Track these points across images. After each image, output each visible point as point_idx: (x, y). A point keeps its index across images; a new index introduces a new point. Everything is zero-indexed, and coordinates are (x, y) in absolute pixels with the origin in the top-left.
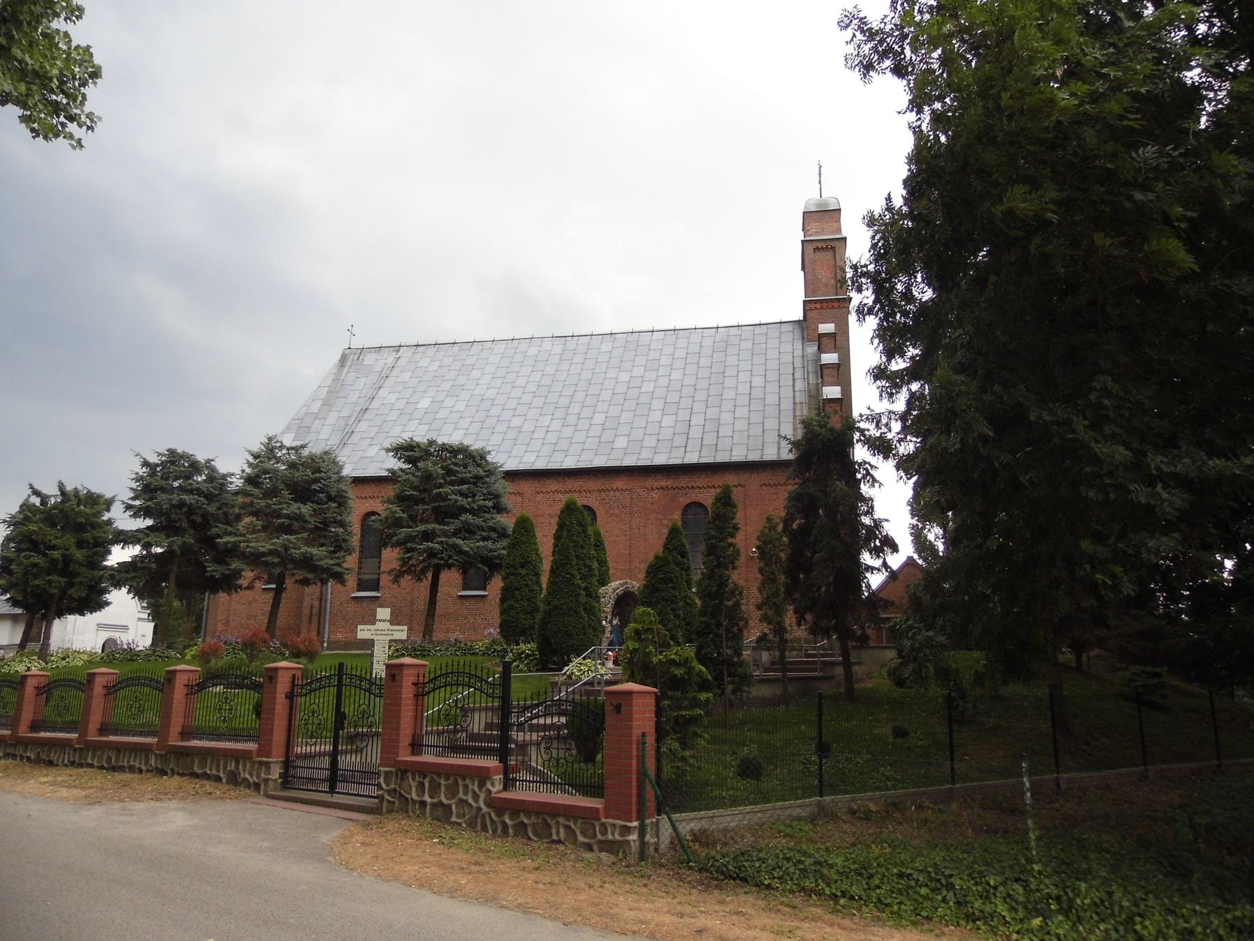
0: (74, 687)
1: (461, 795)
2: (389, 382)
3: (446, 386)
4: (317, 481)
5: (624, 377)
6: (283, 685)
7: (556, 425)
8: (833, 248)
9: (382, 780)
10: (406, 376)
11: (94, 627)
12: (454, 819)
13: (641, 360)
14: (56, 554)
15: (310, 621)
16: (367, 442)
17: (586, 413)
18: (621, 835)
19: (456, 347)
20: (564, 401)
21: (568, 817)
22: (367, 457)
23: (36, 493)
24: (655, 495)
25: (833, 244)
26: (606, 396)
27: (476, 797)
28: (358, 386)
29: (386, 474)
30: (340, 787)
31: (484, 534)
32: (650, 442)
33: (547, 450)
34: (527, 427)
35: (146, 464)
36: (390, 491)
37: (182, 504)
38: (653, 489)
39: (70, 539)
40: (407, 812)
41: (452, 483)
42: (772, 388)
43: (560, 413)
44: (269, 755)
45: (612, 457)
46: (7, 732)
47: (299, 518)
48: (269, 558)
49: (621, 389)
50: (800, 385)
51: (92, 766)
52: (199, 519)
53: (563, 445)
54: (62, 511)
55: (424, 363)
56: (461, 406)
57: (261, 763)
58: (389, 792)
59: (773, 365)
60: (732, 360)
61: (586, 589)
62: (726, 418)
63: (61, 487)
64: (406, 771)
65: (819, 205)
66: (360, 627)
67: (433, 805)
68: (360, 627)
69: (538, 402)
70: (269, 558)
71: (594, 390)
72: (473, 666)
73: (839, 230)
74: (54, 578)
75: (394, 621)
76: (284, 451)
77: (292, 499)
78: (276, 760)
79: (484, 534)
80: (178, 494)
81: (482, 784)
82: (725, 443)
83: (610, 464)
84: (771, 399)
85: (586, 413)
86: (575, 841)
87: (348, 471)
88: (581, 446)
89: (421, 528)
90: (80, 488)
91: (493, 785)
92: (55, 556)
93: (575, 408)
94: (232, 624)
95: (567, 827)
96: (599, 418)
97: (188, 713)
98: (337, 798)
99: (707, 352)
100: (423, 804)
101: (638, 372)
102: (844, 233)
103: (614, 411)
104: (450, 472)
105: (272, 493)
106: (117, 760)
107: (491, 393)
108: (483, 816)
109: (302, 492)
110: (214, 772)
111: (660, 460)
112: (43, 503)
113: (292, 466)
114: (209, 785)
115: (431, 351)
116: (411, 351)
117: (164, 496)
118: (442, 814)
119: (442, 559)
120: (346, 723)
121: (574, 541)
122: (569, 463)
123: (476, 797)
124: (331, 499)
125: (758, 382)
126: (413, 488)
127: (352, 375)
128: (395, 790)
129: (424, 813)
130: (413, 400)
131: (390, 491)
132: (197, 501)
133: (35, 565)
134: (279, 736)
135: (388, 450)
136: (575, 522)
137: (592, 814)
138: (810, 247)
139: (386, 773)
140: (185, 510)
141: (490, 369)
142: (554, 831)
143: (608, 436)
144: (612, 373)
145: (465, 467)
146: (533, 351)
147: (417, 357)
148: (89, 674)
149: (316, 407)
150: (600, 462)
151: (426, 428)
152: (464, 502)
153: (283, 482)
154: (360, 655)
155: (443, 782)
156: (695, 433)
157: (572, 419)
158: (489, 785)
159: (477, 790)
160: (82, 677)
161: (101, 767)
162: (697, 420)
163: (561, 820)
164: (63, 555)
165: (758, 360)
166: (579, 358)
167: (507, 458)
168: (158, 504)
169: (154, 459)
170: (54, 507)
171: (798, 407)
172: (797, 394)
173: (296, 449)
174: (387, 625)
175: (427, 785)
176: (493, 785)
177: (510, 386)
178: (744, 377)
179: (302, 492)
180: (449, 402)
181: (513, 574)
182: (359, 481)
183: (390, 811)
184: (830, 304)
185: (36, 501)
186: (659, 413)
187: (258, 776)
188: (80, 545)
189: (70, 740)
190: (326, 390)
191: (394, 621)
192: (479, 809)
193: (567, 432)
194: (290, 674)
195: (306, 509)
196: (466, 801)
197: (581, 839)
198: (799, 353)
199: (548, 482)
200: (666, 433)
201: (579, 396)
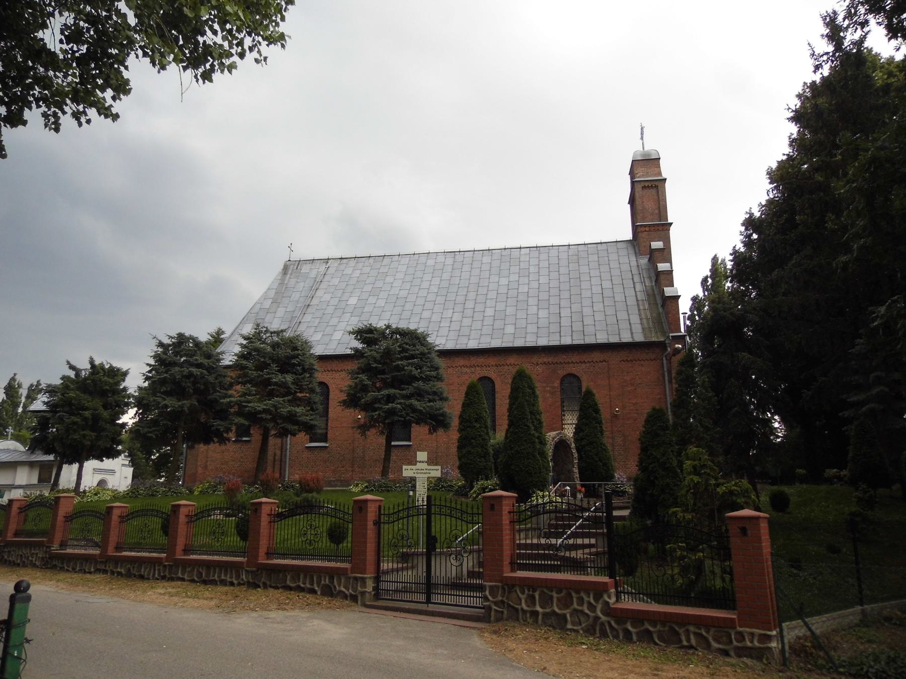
0: (96, 516)
1: (575, 606)
2: (323, 286)
3: (368, 288)
4: (297, 356)
5: (504, 281)
6: (371, 515)
7: (457, 317)
8: (656, 187)
9: (487, 593)
10: (336, 281)
11: (91, 471)
12: (569, 626)
13: (514, 269)
14: (87, 414)
15: (274, 465)
16: (313, 329)
17: (479, 308)
18: (759, 642)
19: (371, 260)
20: (460, 299)
21: (698, 626)
22: (331, 337)
23: (72, 367)
24: (539, 369)
25: (656, 183)
26: (492, 295)
27: (592, 607)
28: (299, 288)
29: (349, 352)
30: (435, 598)
31: (431, 397)
32: (532, 328)
33: (453, 335)
34: (436, 318)
35: (161, 344)
36: (353, 366)
37: (191, 375)
38: (538, 364)
39: (97, 403)
40: (518, 620)
41: (407, 358)
42: (618, 289)
43: (459, 308)
44: (364, 571)
45: (505, 340)
46: (96, 552)
47: (284, 385)
48: (264, 416)
49: (503, 290)
50: (639, 287)
51: (183, 580)
52: (202, 387)
53: (465, 331)
54: (93, 381)
55: (348, 271)
56: (381, 303)
57: (356, 579)
58: (496, 603)
59: (616, 272)
60: (584, 269)
61: (538, 438)
62: (587, 311)
63: (92, 362)
64: (513, 586)
65: (644, 155)
66: (404, 467)
67: (545, 615)
68: (404, 467)
69: (440, 300)
70: (264, 416)
71: (483, 291)
72: (448, 500)
73: (660, 174)
74: (87, 432)
75: (431, 461)
76: (268, 335)
77: (278, 371)
78: (369, 575)
79: (431, 397)
80: (184, 366)
81: (598, 597)
82: (590, 330)
83: (504, 345)
84: (619, 297)
85: (479, 308)
86: (708, 646)
87: (318, 350)
88: (479, 332)
89: (385, 392)
90: (105, 363)
91: (609, 597)
92: (78, 415)
93: (470, 305)
94: (210, 468)
95: (698, 635)
96: (490, 312)
97: (271, 536)
98: (431, 608)
99: (564, 263)
100: (535, 614)
101: (514, 277)
102: (664, 175)
103: (500, 307)
104: (404, 350)
105: (261, 367)
106: (208, 574)
107: (403, 293)
108: (602, 624)
109: (285, 365)
110: (308, 586)
111: (543, 342)
112: (77, 375)
113: (275, 346)
114: (310, 598)
115: (352, 263)
116: (336, 264)
117: (177, 369)
118: (557, 623)
119: (401, 416)
120: (438, 545)
121: (527, 401)
122: (472, 345)
123: (592, 607)
124: (304, 370)
125: (607, 284)
126: (376, 361)
127: (293, 281)
128: (502, 602)
129: (536, 621)
130: (344, 298)
131: (353, 366)
132: (202, 373)
133: (74, 423)
134: (370, 556)
135: (350, 333)
136: (521, 387)
137: (731, 623)
138: (638, 187)
139: (491, 587)
140: (192, 379)
141: (400, 276)
142: (683, 638)
143: (498, 324)
144: (494, 278)
145: (414, 346)
146: (431, 262)
147: (342, 267)
148: (174, 506)
149: (267, 304)
150: (496, 343)
151: (357, 319)
152: (416, 372)
153: (270, 358)
154: (333, 491)
155: (555, 595)
156: (565, 322)
157: (469, 312)
158: (606, 597)
159: (592, 601)
160: (103, 509)
161: (193, 581)
162: (565, 313)
163: (692, 628)
164: (93, 415)
165: (604, 268)
166: (466, 268)
167: (441, 340)
168: (172, 375)
169: (167, 341)
170: (86, 379)
171: (640, 303)
172: (638, 293)
173: (278, 333)
174: (425, 466)
175: (537, 597)
176: (609, 597)
177: (417, 288)
178: (596, 281)
179: (285, 365)
180: (372, 300)
181: (469, 427)
182: (323, 358)
183: (498, 620)
184: (656, 228)
185: (72, 374)
186: (535, 308)
187: (355, 590)
188: (105, 407)
189: (161, 559)
190: (274, 291)
191: (431, 461)
192: (597, 618)
193: (467, 322)
194: (378, 504)
195: (289, 378)
196: (582, 612)
197: (715, 645)
198: (634, 263)
199: (456, 359)
200: (543, 322)
201: (472, 295)
